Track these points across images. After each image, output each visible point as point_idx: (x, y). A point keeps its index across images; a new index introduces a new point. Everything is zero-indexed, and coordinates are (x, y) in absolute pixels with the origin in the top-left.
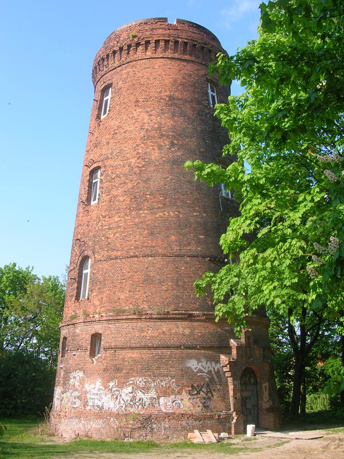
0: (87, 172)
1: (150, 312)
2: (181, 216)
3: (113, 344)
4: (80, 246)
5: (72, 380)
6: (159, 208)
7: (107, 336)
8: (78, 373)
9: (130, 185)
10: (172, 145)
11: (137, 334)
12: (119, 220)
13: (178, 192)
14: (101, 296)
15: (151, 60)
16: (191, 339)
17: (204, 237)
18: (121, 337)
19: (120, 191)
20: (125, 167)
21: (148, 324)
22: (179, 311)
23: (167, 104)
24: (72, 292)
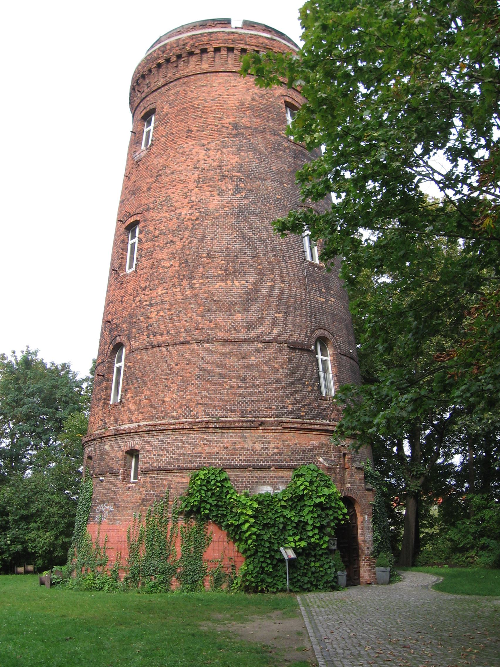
2: (250, 287)
3: (155, 465)
4: (110, 331)
6: (219, 275)
8: (107, 505)
9: (180, 245)
10: (238, 189)
11: (189, 450)
13: (245, 253)
14: (138, 398)
15: (208, 75)
19: (164, 254)
21: (204, 436)
24: (100, 393)
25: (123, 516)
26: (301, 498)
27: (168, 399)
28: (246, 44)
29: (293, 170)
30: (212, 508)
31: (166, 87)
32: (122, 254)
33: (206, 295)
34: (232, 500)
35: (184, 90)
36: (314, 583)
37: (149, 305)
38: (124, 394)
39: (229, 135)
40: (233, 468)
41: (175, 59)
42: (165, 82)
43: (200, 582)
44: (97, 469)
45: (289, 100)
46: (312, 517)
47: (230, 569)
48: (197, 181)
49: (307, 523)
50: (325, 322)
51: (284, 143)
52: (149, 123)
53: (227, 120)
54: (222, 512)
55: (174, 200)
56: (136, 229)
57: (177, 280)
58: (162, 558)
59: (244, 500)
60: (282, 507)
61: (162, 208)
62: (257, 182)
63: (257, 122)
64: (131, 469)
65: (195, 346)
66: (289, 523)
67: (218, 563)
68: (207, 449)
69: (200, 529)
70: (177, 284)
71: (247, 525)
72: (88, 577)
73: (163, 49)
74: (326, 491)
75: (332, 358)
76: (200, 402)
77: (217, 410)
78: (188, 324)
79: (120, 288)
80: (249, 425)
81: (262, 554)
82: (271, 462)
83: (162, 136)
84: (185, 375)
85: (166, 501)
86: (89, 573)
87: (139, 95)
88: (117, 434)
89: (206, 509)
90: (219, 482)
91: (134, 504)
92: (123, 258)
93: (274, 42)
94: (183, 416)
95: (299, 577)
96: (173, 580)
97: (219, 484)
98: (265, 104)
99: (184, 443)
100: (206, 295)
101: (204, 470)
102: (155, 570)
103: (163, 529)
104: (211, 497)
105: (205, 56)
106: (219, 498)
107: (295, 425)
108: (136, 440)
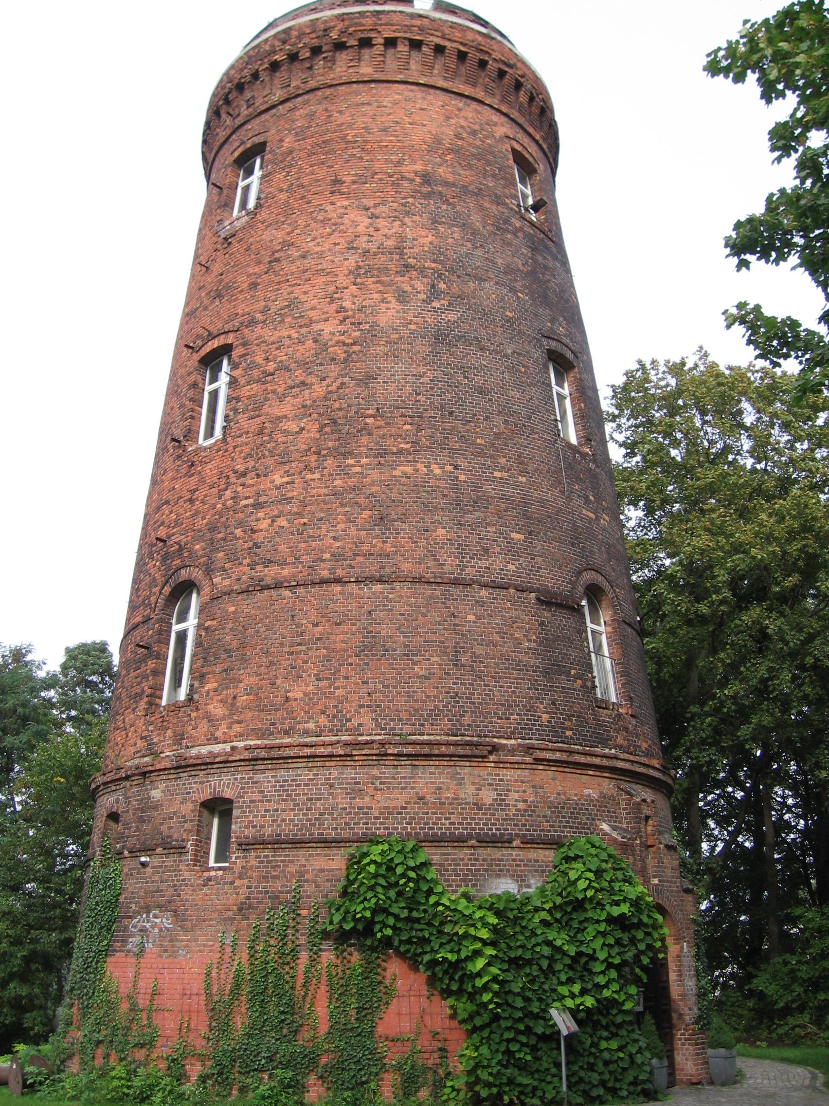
0: (189, 363)
1: (378, 737)
2: (462, 477)
3: (268, 831)
4: (164, 559)
5: (136, 940)
6: (401, 452)
7: (249, 807)
8: (155, 916)
9: (319, 390)
10: (434, 293)
11: (343, 802)
12: (287, 483)
13: (451, 413)
14: (230, 691)
15: (373, 85)
16: (498, 819)
17: (522, 537)
18: (293, 810)
19: (288, 407)
20: (303, 343)
21: (375, 772)
22: (464, 735)
23: (416, 191)
24: (139, 684)
25: (196, 940)
26: (579, 905)
27: (296, 693)
28: (443, 37)
29: (532, 271)
30: (399, 925)
31: (289, 105)
32: (193, 410)
33: (374, 489)
34: (440, 908)
35: (326, 110)
36: (610, 1085)
37: (253, 506)
38: (196, 684)
39: (415, 193)
40: (436, 840)
41: (308, 55)
42: (286, 96)
43: (373, 1085)
44: (133, 840)
45: (518, 147)
46: (604, 944)
47: (436, 1055)
48: (355, 272)
49: (593, 958)
50: (598, 558)
51: (513, 220)
52: (249, 172)
53: (410, 168)
54: (420, 934)
55: (307, 306)
56: (221, 362)
57: (314, 458)
58: (285, 1031)
59: (467, 907)
60: (544, 923)
61: (282, 321)
62: (471, 283)
63: (466, 176)
64: (210, 839)
65: (353, 588)
66: (558, 957)
67: (409, 1044)
68: (383, 800)
69: (370, 969)
70: (313, 464)
71: (480, 963)
72: (113, 1073)
73: (285, 37)
74: (632, 892)
75: (609, 629)
76: (366, 701)
77: (400, 720)
78: (338, 544)
79: (188, 475)
80: (468, 752)
81: (509, 1024)
82: (512, 830)
83: (281, 190)
84: (332, 646)
85: (294, 907)
86: (113, 1063)
87: (228, 123)
88: (182, 767)
89: (385, 926)
90: (413, 869)
91: (221, 914)
92: (194, 417)
93: (493, 42)
94: (331, 731)
95: (582, 1074)
96: (311, 1082)
97: (412, 874)
98: (478, 147)
99: (332, 786)
100: (374, 489)
101: (378, 843)
102: (270, 1059)
103: (287, 968)
104: (396, 901)
105: (366, 53)
106: (412, 904)
107: (558, 756)
108: (225, 778)
